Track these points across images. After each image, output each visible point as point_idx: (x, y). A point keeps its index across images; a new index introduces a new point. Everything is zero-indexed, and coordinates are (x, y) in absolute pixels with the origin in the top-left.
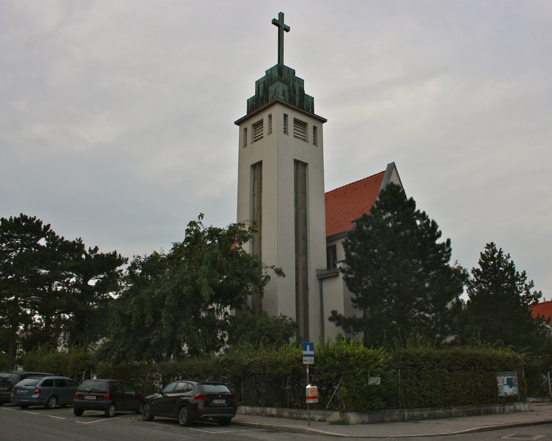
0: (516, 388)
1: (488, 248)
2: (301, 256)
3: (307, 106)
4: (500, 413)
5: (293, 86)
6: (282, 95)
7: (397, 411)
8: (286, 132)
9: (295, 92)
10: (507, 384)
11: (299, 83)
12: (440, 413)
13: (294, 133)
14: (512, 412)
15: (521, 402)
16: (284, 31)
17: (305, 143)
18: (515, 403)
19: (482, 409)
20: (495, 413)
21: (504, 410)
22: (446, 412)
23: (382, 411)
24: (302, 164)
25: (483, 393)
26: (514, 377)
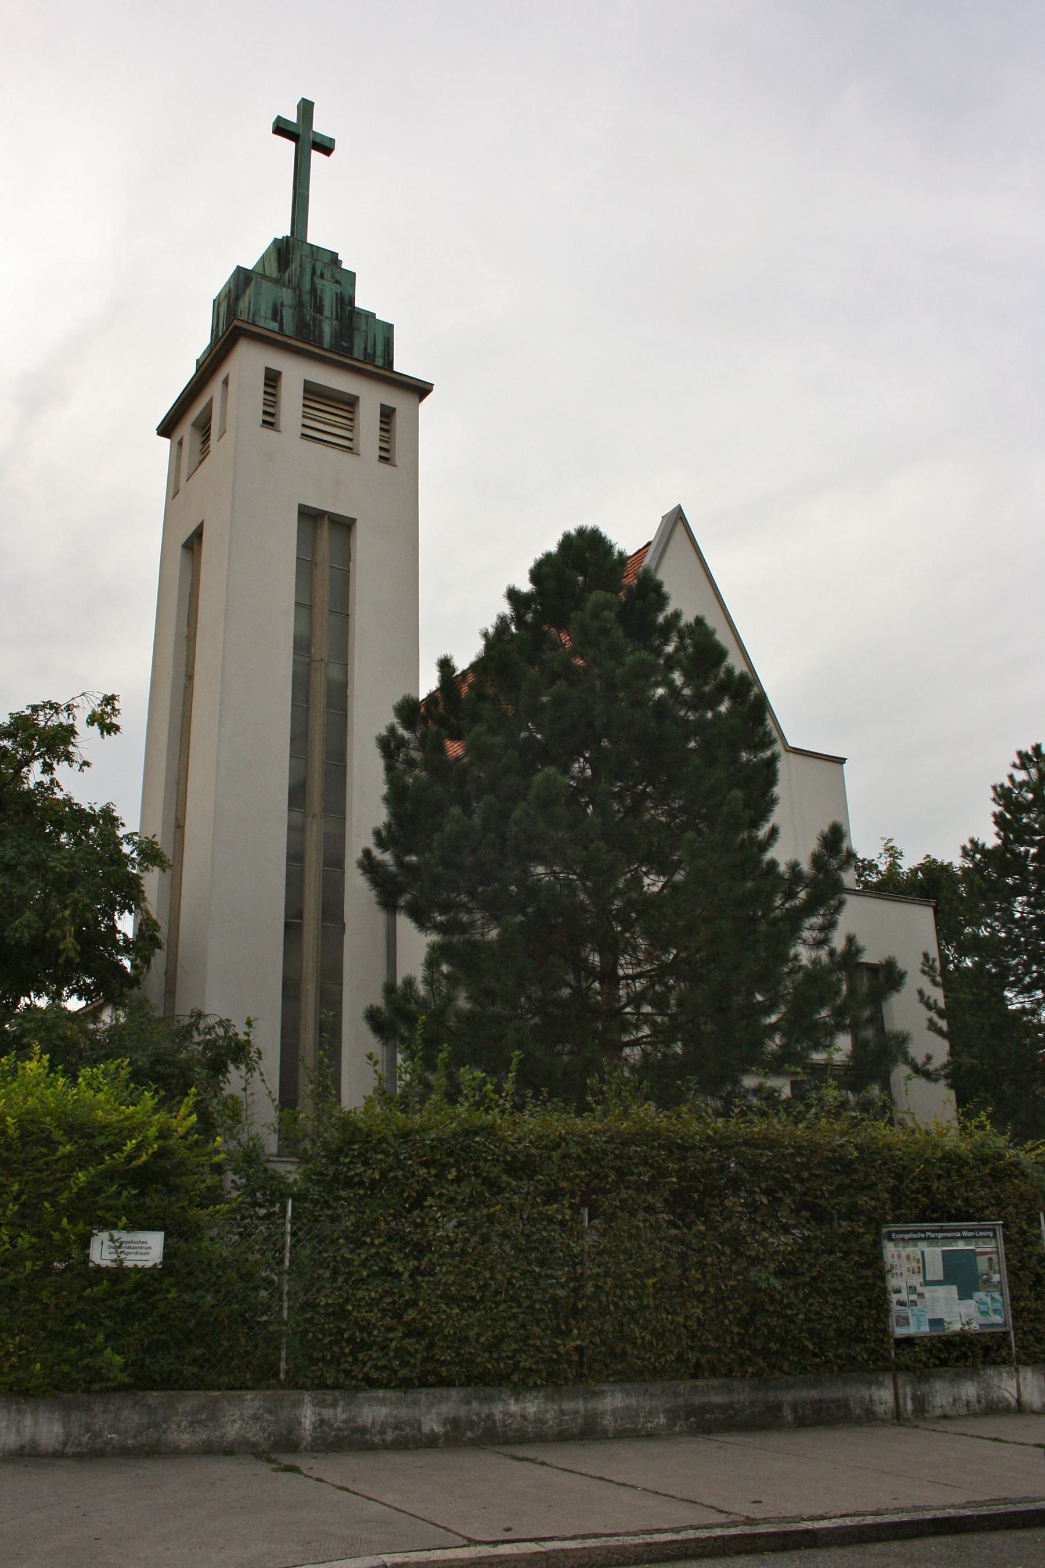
0: (996, 1295)
1: (1023, 767)
2: (314, 816)
3: (366, 349)
4: (898, 1417)
5: (313, 290)
6: (270, 314)
7: (252, 1402)
8: (270, 422)
9: (319, 309)
10: (948, 1279)
11: (337, 282)
12: (524, 1417)
13: (304, 426)
14: (975, 1415)
15: (1026, 1364)
16: (313, 152)
17: (346, 457)
18: (990, 1372)
19: (789, 1396)
20: (869, 1417)
21: (921, 1405)
22: (562, 1412)
23: (154, 1397)
24: (329, 518)
25: (791, 1320)
26: (989, 1247)
